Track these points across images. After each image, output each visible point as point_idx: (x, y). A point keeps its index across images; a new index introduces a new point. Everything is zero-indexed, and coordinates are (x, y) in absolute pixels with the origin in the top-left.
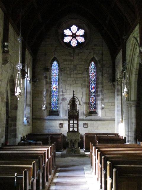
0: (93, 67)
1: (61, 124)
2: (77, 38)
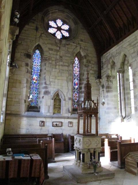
0: (76, 62)
1: (43, 122)
2: (62, 31)
